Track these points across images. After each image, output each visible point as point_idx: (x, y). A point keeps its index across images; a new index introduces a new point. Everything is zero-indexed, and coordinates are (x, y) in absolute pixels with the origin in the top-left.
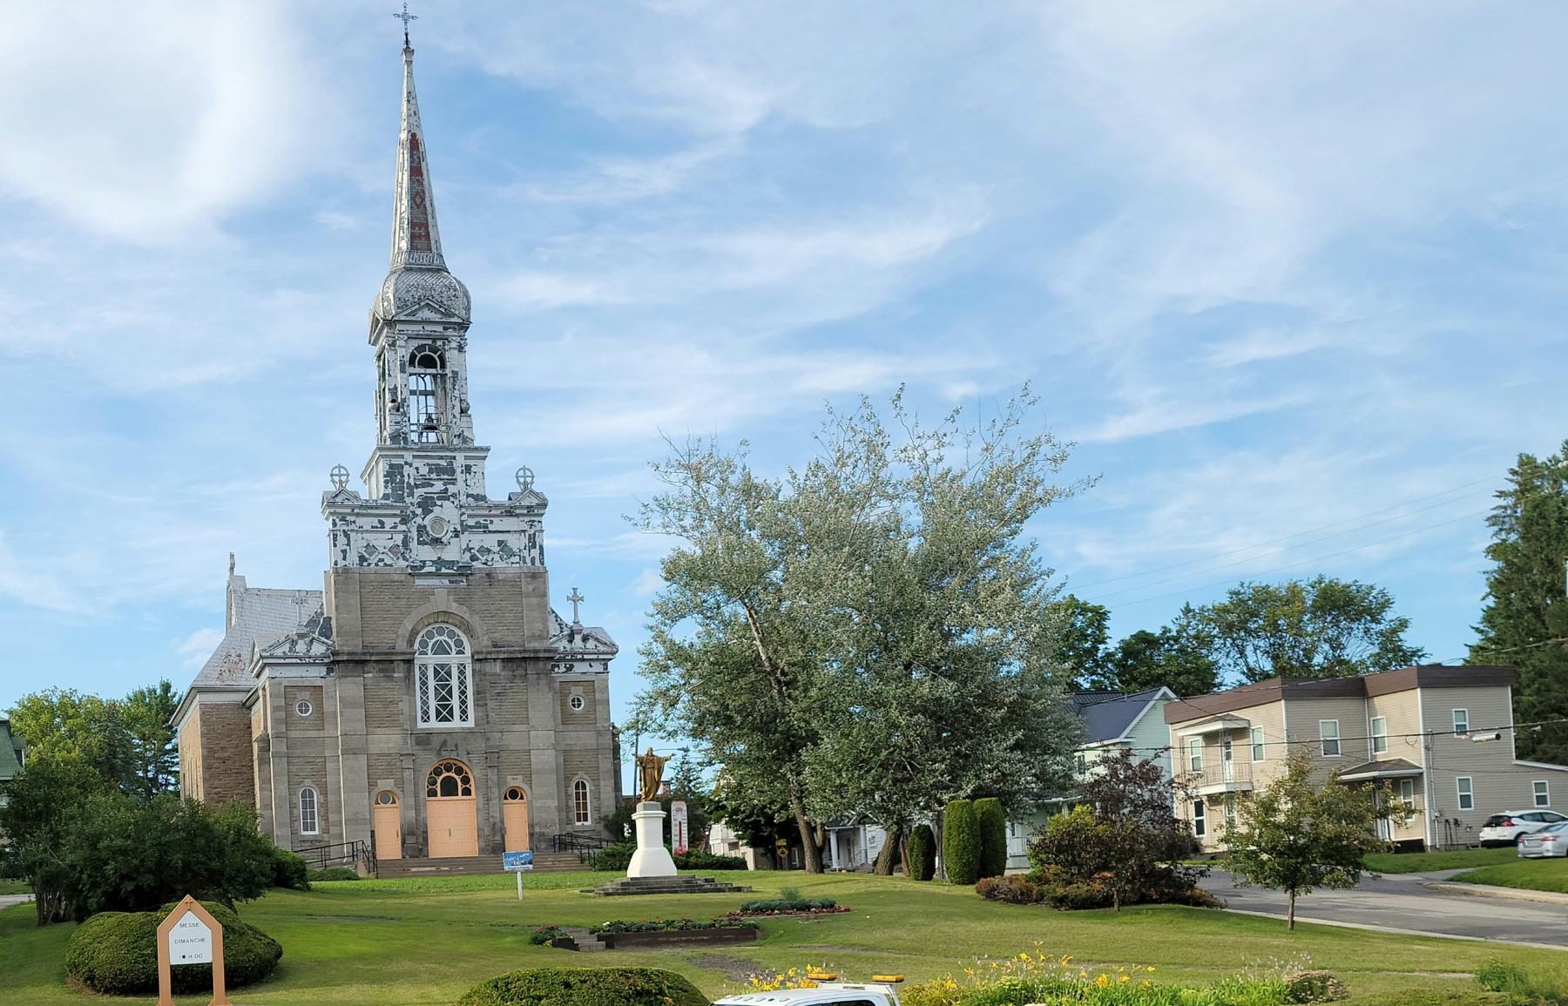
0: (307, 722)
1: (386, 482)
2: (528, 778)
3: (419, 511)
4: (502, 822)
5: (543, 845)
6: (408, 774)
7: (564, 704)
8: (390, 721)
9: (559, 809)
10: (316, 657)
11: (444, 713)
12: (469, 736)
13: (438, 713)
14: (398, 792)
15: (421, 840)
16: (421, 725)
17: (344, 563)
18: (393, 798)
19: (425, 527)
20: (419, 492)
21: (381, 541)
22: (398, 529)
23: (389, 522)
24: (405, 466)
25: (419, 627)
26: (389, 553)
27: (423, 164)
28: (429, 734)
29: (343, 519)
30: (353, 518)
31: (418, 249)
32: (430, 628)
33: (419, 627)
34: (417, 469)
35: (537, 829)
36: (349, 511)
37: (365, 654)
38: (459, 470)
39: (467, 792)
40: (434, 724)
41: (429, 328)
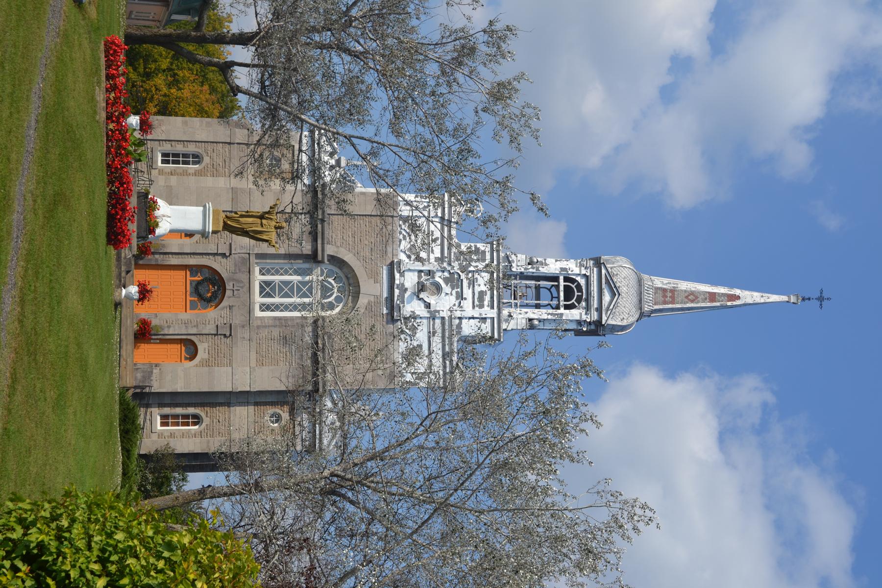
2: (206, 363)
12: (247, 308)
13: (268, 283)
31: (655, 293)
40: (258, 277)
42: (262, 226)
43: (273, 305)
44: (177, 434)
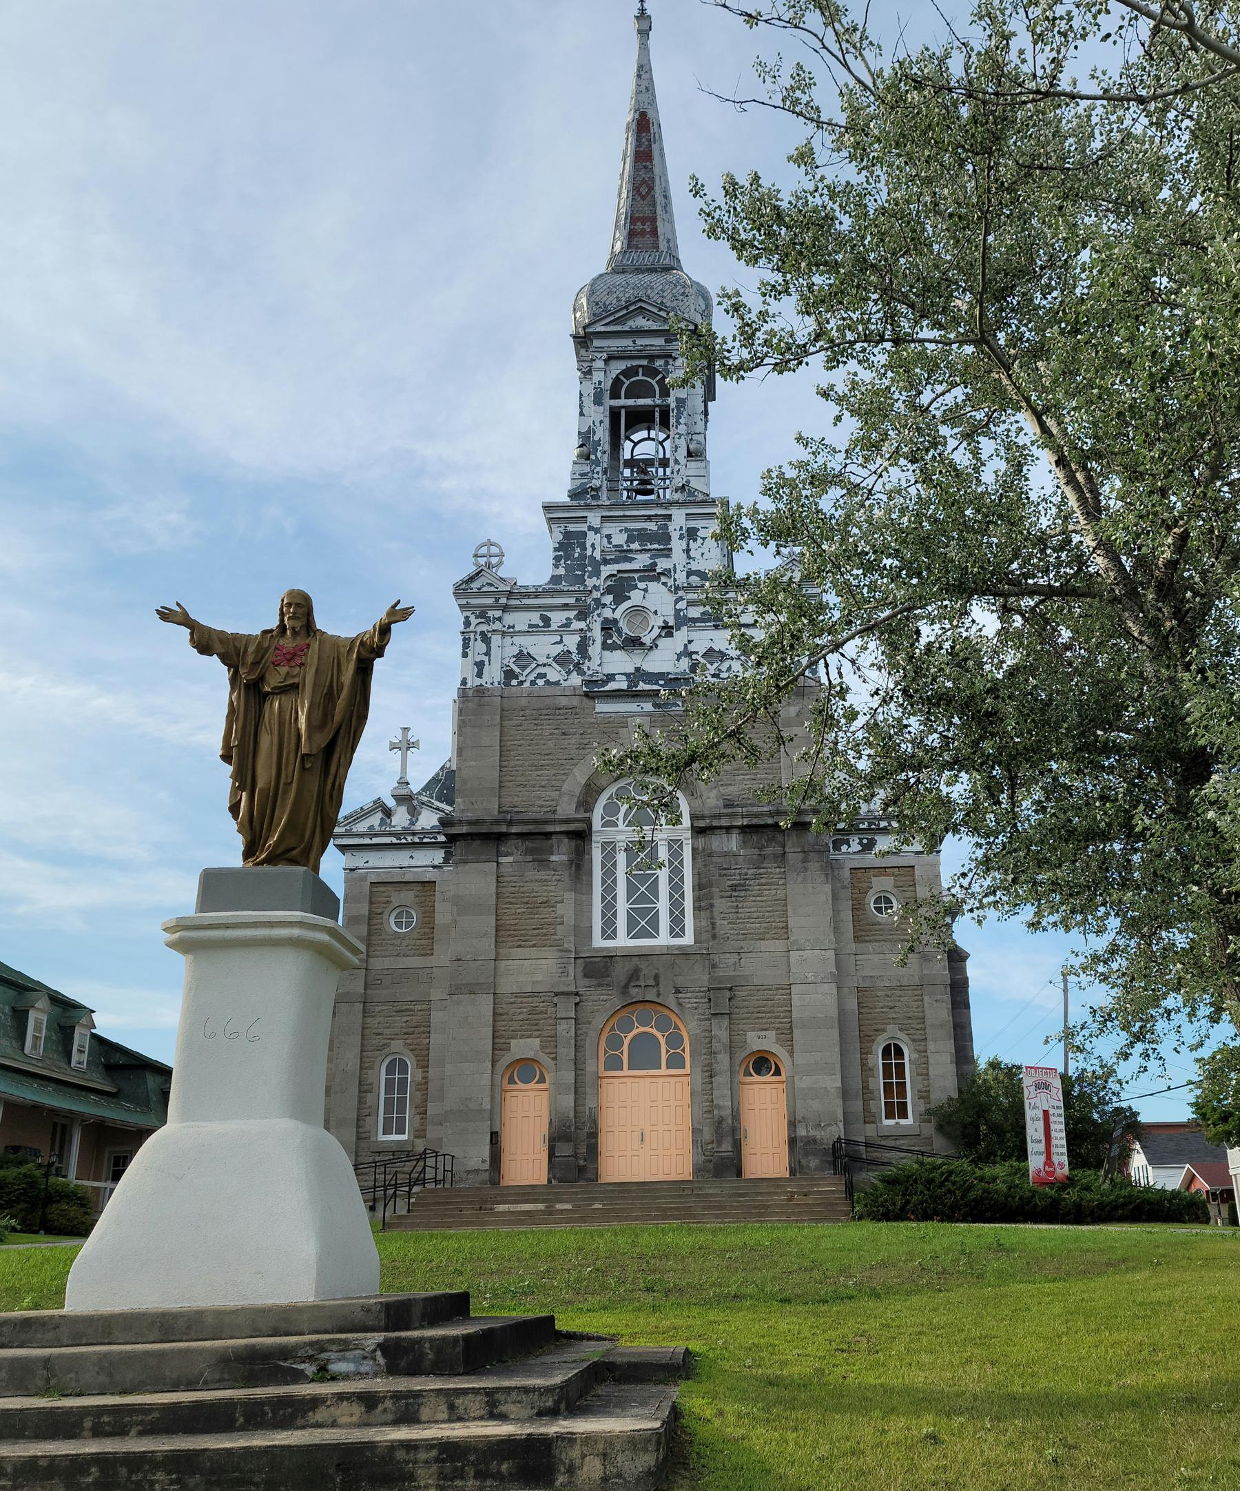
0: (405, 943)
1: (557, 559)
2: (787, 1035)
3: (608, 599)
4: (736, 1115)
5: (813, 1162)
6: (565, 1029)
7: (858, 907)
8: (542, 936)
9: (845, 1094)
10: (424, 833)
11: (643, 922)
12: (679, 961)
14: (546, 1060)
15: (583, 1150)
16: (598, 942)
17: (478, 681)
18: (541, 1071)
19: (615, 621)
20: (606, 570)
21: (543, 647)
22: (573, 627)
23: (557, 618)
24: (589, 533)
25: (603, 781)
26: (554, 664)
27: (655, 147)
28: (610, 958)
29: (482, 615)
30: (498, 614)
32: (622, 783)
33: (603, 781)
34: (609, 537)
35: (802, 1132)
36: (490, 601)
37: (497, 822)
38: (675, 536)
39: (676, 1062)
40: (623, 941)
41: (641, 342)
42: (295, 687)
43: (671, 913)
44: (920, 1086)
